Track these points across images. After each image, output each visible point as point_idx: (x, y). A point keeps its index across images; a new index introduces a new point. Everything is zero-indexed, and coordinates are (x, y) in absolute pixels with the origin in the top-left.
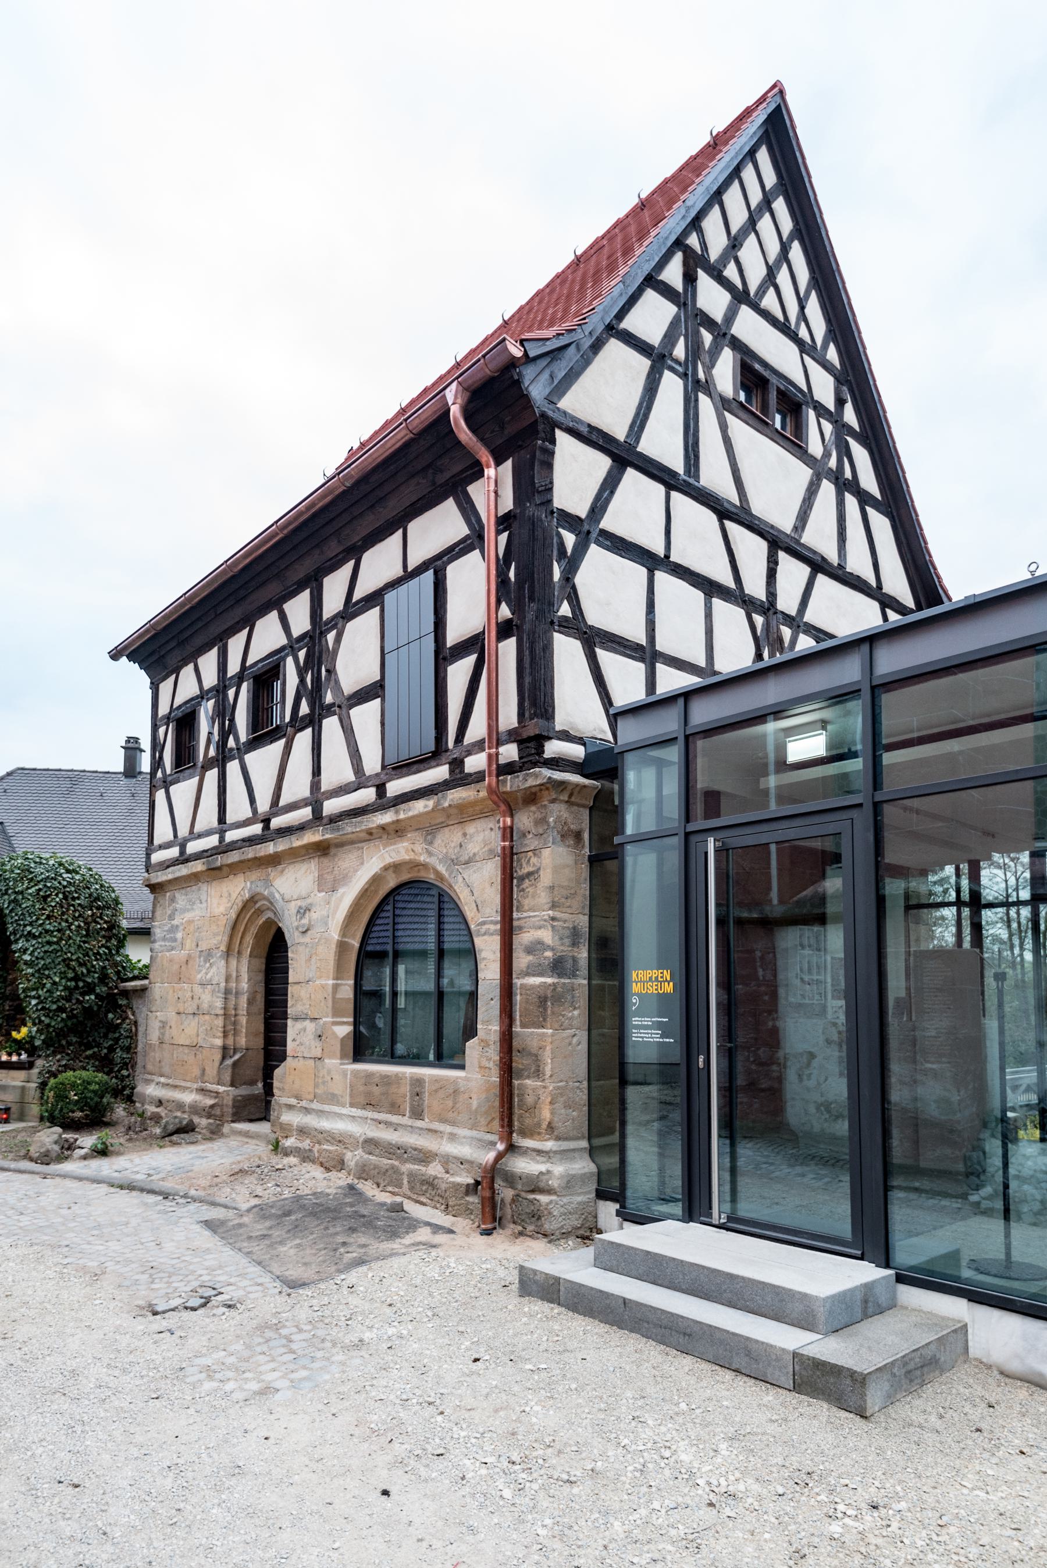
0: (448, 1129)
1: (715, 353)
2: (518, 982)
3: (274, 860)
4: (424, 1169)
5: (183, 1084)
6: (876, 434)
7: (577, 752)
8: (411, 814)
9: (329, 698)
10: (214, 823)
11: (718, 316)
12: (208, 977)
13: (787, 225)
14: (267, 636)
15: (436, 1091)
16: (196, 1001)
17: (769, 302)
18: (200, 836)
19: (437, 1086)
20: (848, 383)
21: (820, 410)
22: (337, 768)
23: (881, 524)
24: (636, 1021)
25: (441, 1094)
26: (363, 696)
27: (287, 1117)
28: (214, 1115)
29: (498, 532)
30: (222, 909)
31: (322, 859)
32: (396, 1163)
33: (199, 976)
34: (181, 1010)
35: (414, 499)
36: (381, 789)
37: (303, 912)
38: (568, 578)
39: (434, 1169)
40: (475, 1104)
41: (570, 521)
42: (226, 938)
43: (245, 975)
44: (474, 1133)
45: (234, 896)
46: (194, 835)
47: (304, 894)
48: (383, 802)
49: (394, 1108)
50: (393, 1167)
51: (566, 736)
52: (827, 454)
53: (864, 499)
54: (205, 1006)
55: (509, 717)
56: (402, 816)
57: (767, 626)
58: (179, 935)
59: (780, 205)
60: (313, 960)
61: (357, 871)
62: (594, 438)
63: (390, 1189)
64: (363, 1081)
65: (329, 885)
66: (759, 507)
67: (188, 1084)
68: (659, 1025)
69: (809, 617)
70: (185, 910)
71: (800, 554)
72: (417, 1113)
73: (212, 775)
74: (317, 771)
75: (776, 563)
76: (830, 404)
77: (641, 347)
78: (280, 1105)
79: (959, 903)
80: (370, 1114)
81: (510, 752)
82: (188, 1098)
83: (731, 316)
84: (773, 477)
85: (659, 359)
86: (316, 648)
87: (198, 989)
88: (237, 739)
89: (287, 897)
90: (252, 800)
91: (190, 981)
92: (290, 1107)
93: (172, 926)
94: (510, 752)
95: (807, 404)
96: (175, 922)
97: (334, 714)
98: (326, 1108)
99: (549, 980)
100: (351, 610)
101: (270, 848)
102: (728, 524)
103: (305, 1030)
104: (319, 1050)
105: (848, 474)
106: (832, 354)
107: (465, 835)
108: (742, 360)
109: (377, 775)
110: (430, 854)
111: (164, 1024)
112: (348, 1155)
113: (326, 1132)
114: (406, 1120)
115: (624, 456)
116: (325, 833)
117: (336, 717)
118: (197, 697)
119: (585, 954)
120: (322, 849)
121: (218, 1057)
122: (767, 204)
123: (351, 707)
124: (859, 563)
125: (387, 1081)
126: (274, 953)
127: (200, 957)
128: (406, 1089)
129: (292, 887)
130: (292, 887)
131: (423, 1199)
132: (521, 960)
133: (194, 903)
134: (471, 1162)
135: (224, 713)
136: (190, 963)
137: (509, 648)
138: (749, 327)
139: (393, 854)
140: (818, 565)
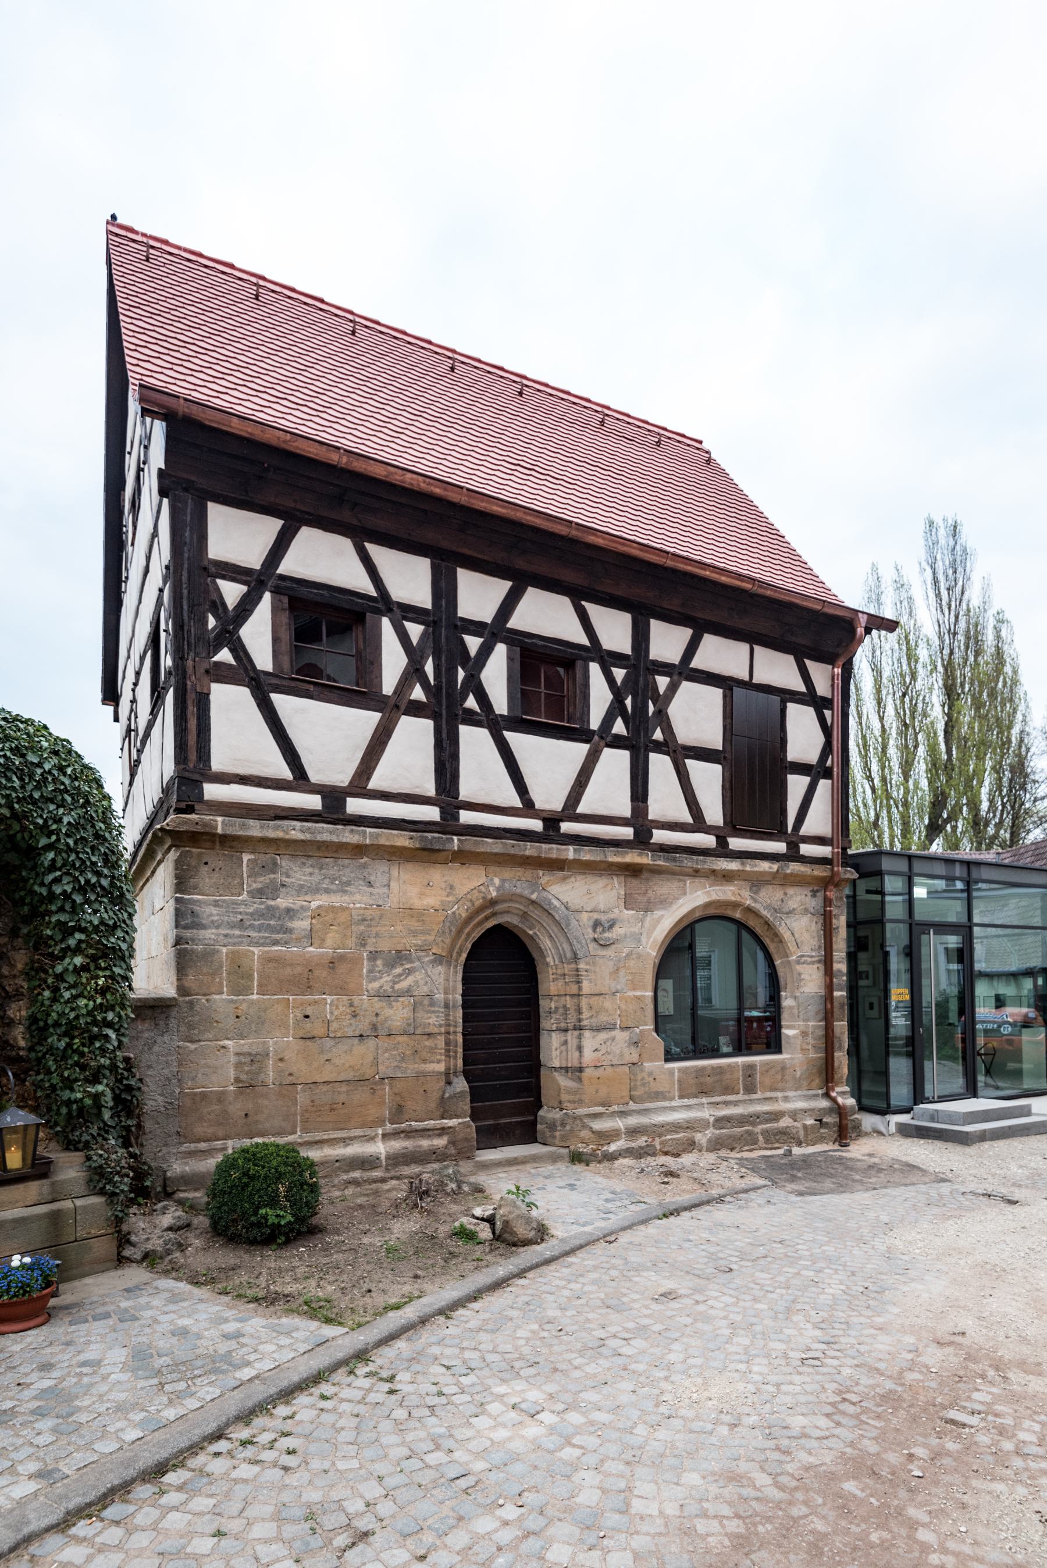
0: (779, 1095)
3: (558, 865)
8: (756, 869)
12: (404, 985)
22: (665, 799)
24: (894, 1014)
25: (772, 1072)
28: (451, 1155)
31: (629, 879)
32: (750, 1128)
35: (763, 632)
36: (722, 841)
39: (785, 1122)
40: (798, 1074)
44: (799, 1093)
48: (722, 850)
49: (729, 1090)
50: (747, 1132)
56: (748, 868)
60: (622, 973)
61: (678, 899)
63: (746, 1148)
64: (694, 1075)
68: (903, 1016)
80: (704, 1100)
103: (613, 1039)
104: (637, 1056)
107: (785, 894)
110: (755, 901)
112: (698, 1137)
113: (668, 1124)
120: (633, 871)
125: (720, 1071)
131: (777, 1145)
134: (810, 1110)
136: (342, 969)
139: (720, 894)
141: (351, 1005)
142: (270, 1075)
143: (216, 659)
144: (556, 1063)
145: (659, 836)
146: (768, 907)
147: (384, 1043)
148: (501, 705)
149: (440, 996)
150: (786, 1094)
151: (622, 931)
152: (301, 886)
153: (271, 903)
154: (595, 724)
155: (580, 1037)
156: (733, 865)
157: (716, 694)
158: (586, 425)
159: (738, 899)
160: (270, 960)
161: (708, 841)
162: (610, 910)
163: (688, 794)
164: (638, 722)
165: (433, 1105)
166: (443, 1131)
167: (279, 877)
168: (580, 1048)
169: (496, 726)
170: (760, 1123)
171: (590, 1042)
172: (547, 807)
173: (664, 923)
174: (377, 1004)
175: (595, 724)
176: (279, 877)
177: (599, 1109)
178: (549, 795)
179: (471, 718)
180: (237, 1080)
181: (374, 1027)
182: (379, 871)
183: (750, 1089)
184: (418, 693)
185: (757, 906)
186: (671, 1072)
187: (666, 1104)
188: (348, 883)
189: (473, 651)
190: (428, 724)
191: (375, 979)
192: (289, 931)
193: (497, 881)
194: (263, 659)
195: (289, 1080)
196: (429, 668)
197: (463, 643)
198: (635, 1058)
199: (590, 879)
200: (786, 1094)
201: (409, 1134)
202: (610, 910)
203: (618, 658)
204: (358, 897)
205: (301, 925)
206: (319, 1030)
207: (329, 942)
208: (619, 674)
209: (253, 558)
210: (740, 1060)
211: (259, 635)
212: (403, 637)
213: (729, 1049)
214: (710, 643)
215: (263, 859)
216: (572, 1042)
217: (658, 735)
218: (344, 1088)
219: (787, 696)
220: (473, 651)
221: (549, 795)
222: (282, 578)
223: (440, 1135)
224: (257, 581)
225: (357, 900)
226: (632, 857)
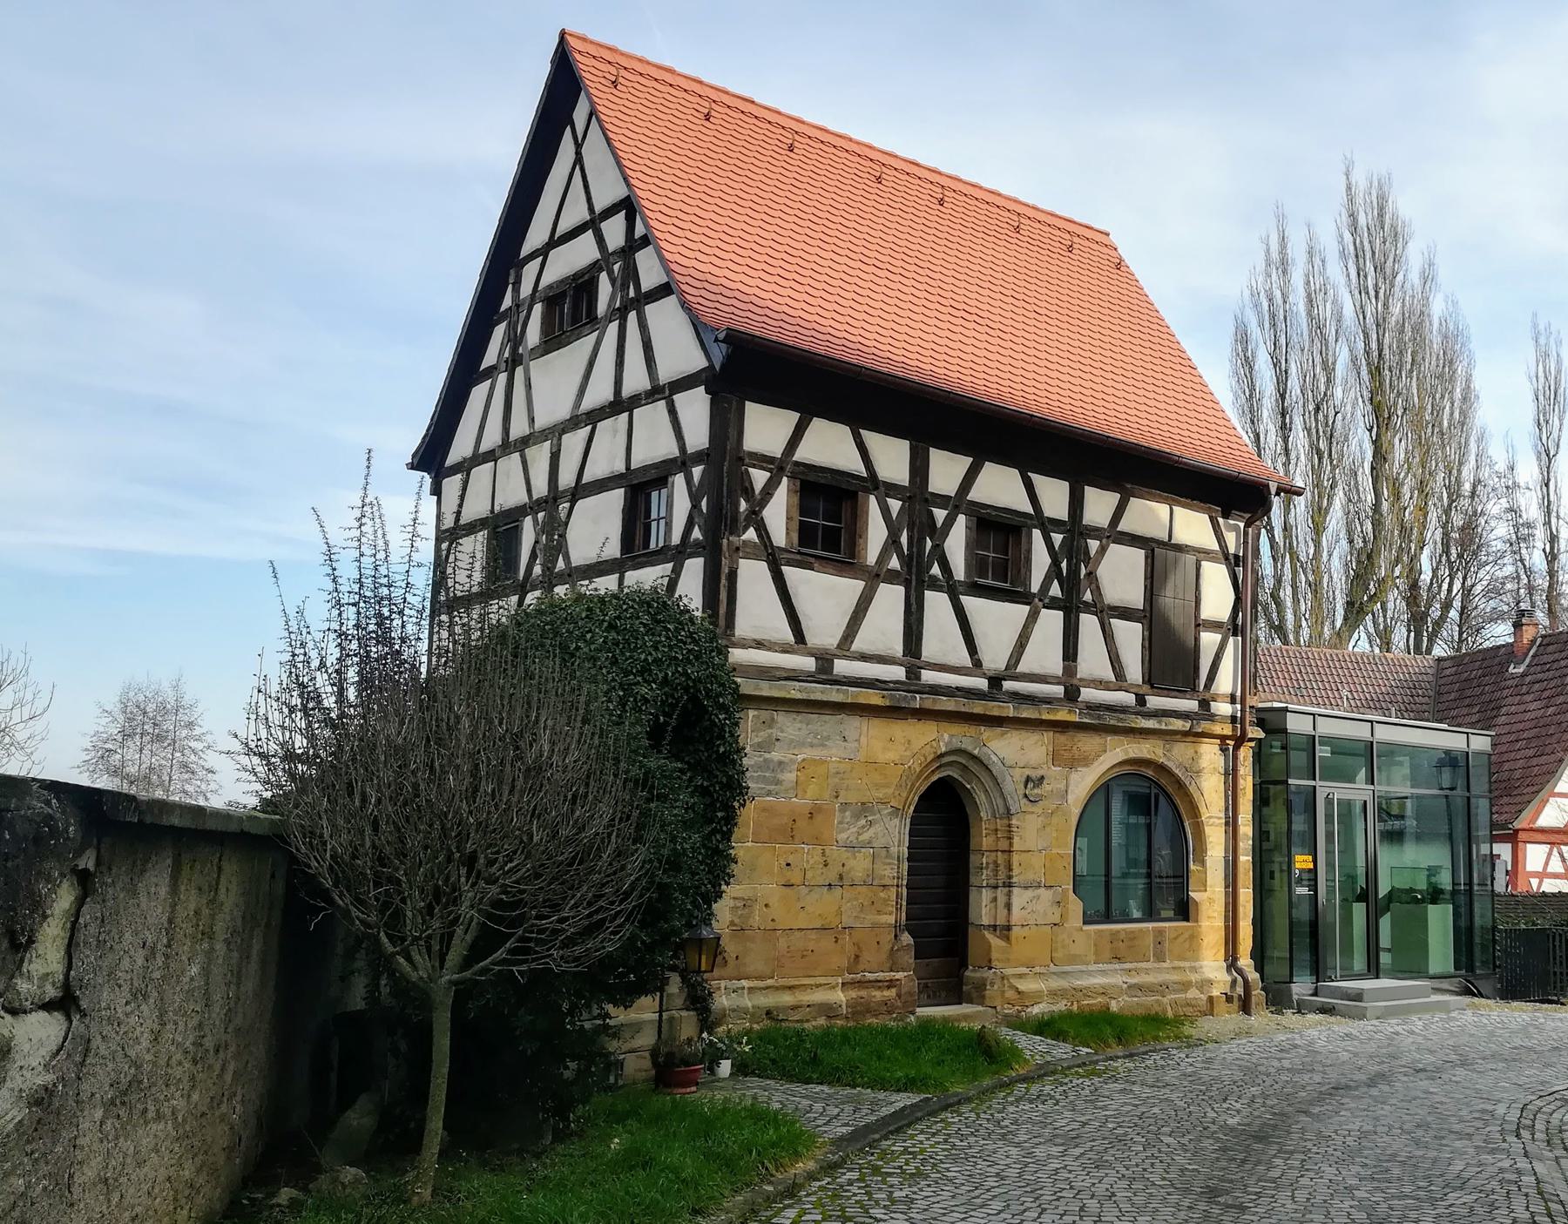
0: (1187, 964)
12: (865, 837)
22: (1093, 659)
25: (1181, 939)
33: (843, 836)
36: (1141, 700)
92: (1021, 976)
98: (1068, 968)
116: (1072, 717)
128: (1150, 940)
129: (1013, 752)
130: (1013, 752)
136: (819, 818)
141: (823, 854)
142: (756, 920)
143: (744, 537)
144: (985, 921)
145: (1088, 694)
146: (1180, 765)
147: (849, 893)
148: (959, 573)
149: (894, 850)
151: (1048, 788)
152: (792, 741)
153: (767, 756)
154: (1035, 587)
155: (1009, 894)
156: (1150, 724)
157: (1139, 555)
160: (764, 810)
161: (1129, 699)
163: (1111, 656)
164: (1071, 584)
165: (884, 956)
166: (891, 984)
167: (775, 732)
168: (1008, 906)
169: (954, 591)
171: (1019, 898)
172: (993, 666)
173: (1083, 782)
174: (845, 854)
175: (1035, 587)
176: (775, 732)
177: (1024, 970)
178: (995, 656)
179: (934, 585)
180: (732, 923)
181: (841, 877)
182: (854, 725)
183: (1160, 958)
184: (894, 563)
185: (1170, 764)
186: (1088, 933)
187: (1083, 968)
188: (828, 738)
189: (940, 522)
190: (901, 590)
191: (843, 831)
192: (778, 782)
193: (946, 737)
194: (779, 535)
195: (770, 926)
196: (904, 539)
197: (931, 516)
199: (1024, 734)
201: (861, 984)
203: (1056, 524)
204: (834, 751)
205: (789, 777)
206: (796, 878)
207: (809, 795)
208: (1058, 538)
209: (775, 448)
210: (1150, 925)
211: (778, 515)
212: (885, 511)
213: (1171, 914)
214: (818, 426)
215: (765, 715)
216: (1002, 899)
217: (1088, 596)
218: (813, 935)
219: (1206, 554)
220: (940, 522)
221: (995, 656)
222: (797, 464)
223: (889, 987)
224: (778, 467)
225: (835, 753)
226: (1062, 715)
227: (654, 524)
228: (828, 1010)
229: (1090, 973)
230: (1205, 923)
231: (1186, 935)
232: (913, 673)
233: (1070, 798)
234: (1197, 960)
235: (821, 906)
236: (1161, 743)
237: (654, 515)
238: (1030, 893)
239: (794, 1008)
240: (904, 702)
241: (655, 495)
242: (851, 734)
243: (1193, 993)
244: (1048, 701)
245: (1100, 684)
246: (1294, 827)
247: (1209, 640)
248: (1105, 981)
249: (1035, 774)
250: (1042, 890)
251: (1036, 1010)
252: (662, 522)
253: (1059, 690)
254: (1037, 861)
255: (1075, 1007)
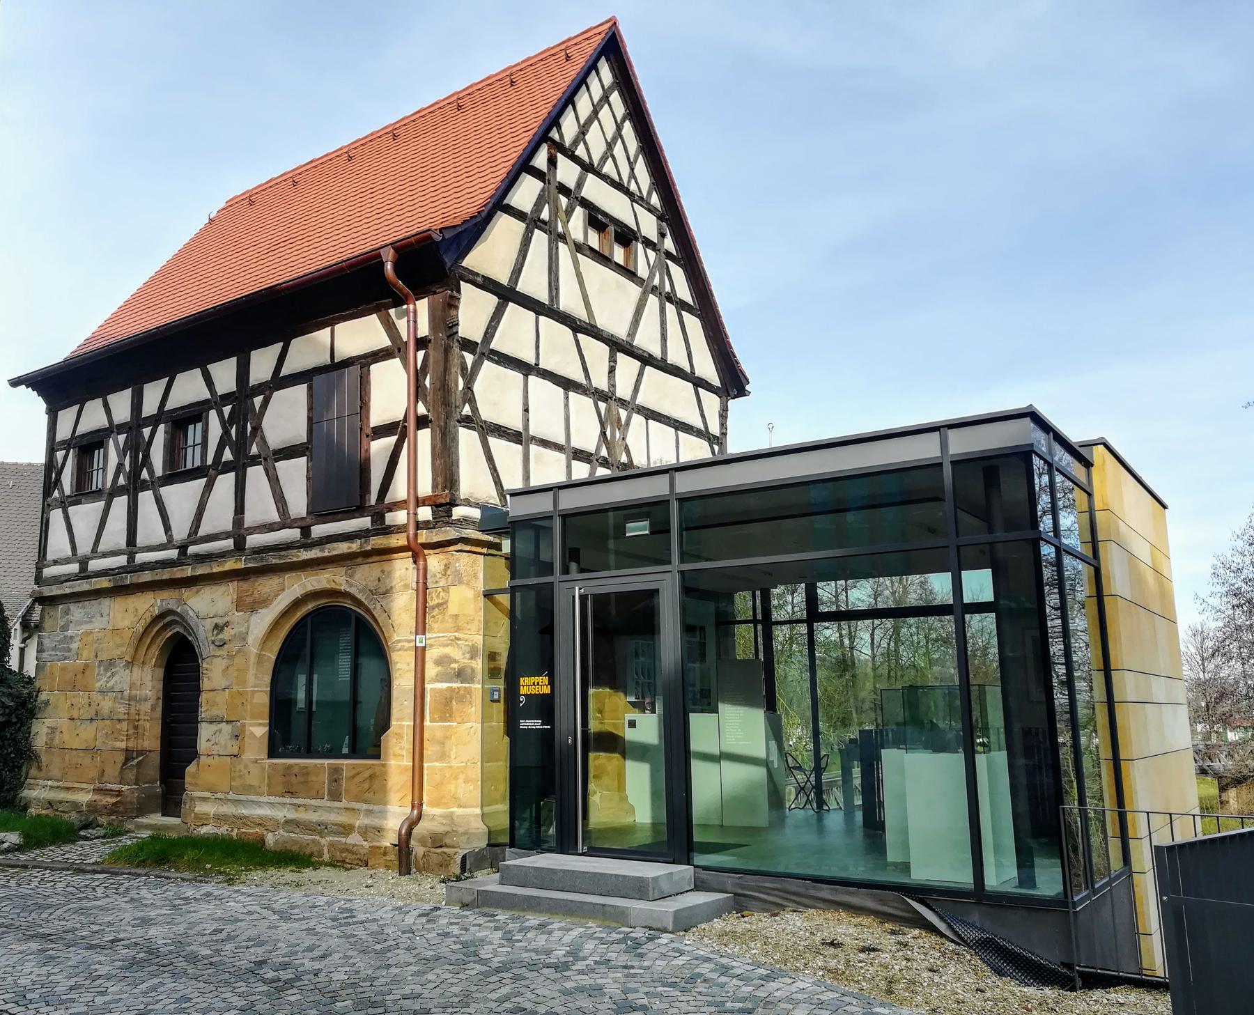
0: (365, 806)
1: (569, 212)
2: (428, 686)
4: (343, 840)
5: (77, 785)
6: (688, 257)
7: (475, 513)
9: (254, 450)
10: (122, 543)
11: (571, 184)
12: (110, 684)
13: (620, 110)
14: (188, 388)
15: (353, 777)
16: (94, 707)
17: (608, 168)
18: (105, 555)
19: (353, 772)
20: (666, 221)
21: (648, 243)
22: (261, 506)
23: (694, 324)
25: (358, 779)
26: (289, 452)
27: (201, 808)
29: (417, 349)
30: (127, 623)
32: (317, 838)
33: (98, 685)
34: (75, 716)
36: (306, 531)
37: (219, 628)
38: (469, 388)
41: (468, 345)
42: (132, 650)
43: (145, 682)
45: (141, 612)
46: (95, 553)
47: (220, 612)
48: (307, 542)
51: (468, 503)
52: (652, 276)
53: (682, 305)
54: (106, 712)
55: (425, 487)
57: (608, 410)
58: (74, 646)
59: (615, 97)
62: (488, 284)
65: (249, 606)
66: (602, 322)
67: (84, 786)
69: (639, 401)
70: (80, 623)
71: (631, 351)
72: (335, 796)
73: (121, 503)
74: (240, 508)
75: (615, 362)
76: (654, 237)
77: (519, 215)
78: (193, 799)
79: (755, 621)
80: (288, 800)
81: (425, 513)
82: (84, 798)
83: (580, 184)
84: (611, 299)
85: (533, 222)
86: (243, 405)
87: (96, 697)
88: (151, 472)
89: (201, 615)
90: (167, 528)
91: (86, 688)
92: (204, 799)
93: (65, 637)
94: (425, 513)
95: (637, 239)
96: (69, 633)
97: (260, 464)
98: (243, 797)
99: (455, 685)
100: (279, 382)
101: (188, 572)
102: (580, 336)
103: (220, 731)
105: (668, 288)
106: (655, 200)
107: (383, 571)
108: (590, 215)
109: (302, 519)
111: (53, 730)
113: (245, 817)
114: (325, 803)
115: (507, 294)
116: (255, 566)
117: (261, 468)
118: (105, 429)
119: (480, 665)
121: (120, 758)
122: (605, 98)
123: (277, 460)
124: (676, 356)
126: (180, 660)
127: (99, 666)
128: (325, 777)
129: (206, 605)
130: (206, 605)
132: (431, 670)
133: (93, 616)
135: (137, 449)
136: (87, 672)
137: (425, 436)
138: (595, 190)
140: (646, 360)
142: (57, 741)
150: (371, 807)
158: (445, 122)
159: (333, 586)
162: (226, 614)
164: (240, 447)
170: (329, 834)
177: (207, 794)
185: (353, 591)
198: (235, 751)
200: (371, 807)
202: (226, 614)
225: (97, 625)
227: (190, 451)
228: (75, 806)
229: (259, 804)
230: (392, 762)
231: (367, 774)
232: (131, 558)
233: (250, 639)
234: (386, 804)
235: (87, 734)
236: (342, 570)
237: (190, 442)
238: (214, 727)
239: (61, 802)
240: (122, 586)
241: (191, 427)
242: (105, 611)
243: (354, 839)
244: (222, 555)
245: (269, 527)
246: (863, 629)
247: (380, 448)
248: (268, 813)
249: (220, 621)
250: (224, 724)
251: (204, 830)
252: (198, 449)
253: (228, 544)
254: (222, 699)
255: (234, 834)
